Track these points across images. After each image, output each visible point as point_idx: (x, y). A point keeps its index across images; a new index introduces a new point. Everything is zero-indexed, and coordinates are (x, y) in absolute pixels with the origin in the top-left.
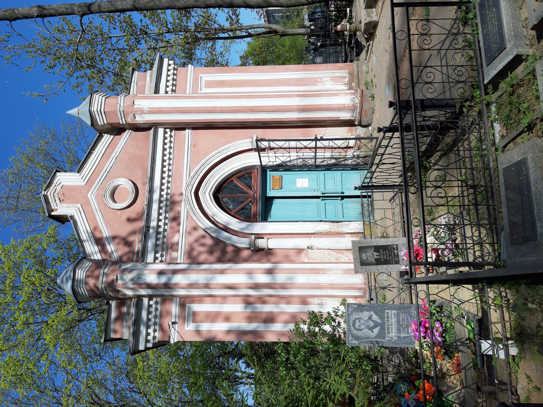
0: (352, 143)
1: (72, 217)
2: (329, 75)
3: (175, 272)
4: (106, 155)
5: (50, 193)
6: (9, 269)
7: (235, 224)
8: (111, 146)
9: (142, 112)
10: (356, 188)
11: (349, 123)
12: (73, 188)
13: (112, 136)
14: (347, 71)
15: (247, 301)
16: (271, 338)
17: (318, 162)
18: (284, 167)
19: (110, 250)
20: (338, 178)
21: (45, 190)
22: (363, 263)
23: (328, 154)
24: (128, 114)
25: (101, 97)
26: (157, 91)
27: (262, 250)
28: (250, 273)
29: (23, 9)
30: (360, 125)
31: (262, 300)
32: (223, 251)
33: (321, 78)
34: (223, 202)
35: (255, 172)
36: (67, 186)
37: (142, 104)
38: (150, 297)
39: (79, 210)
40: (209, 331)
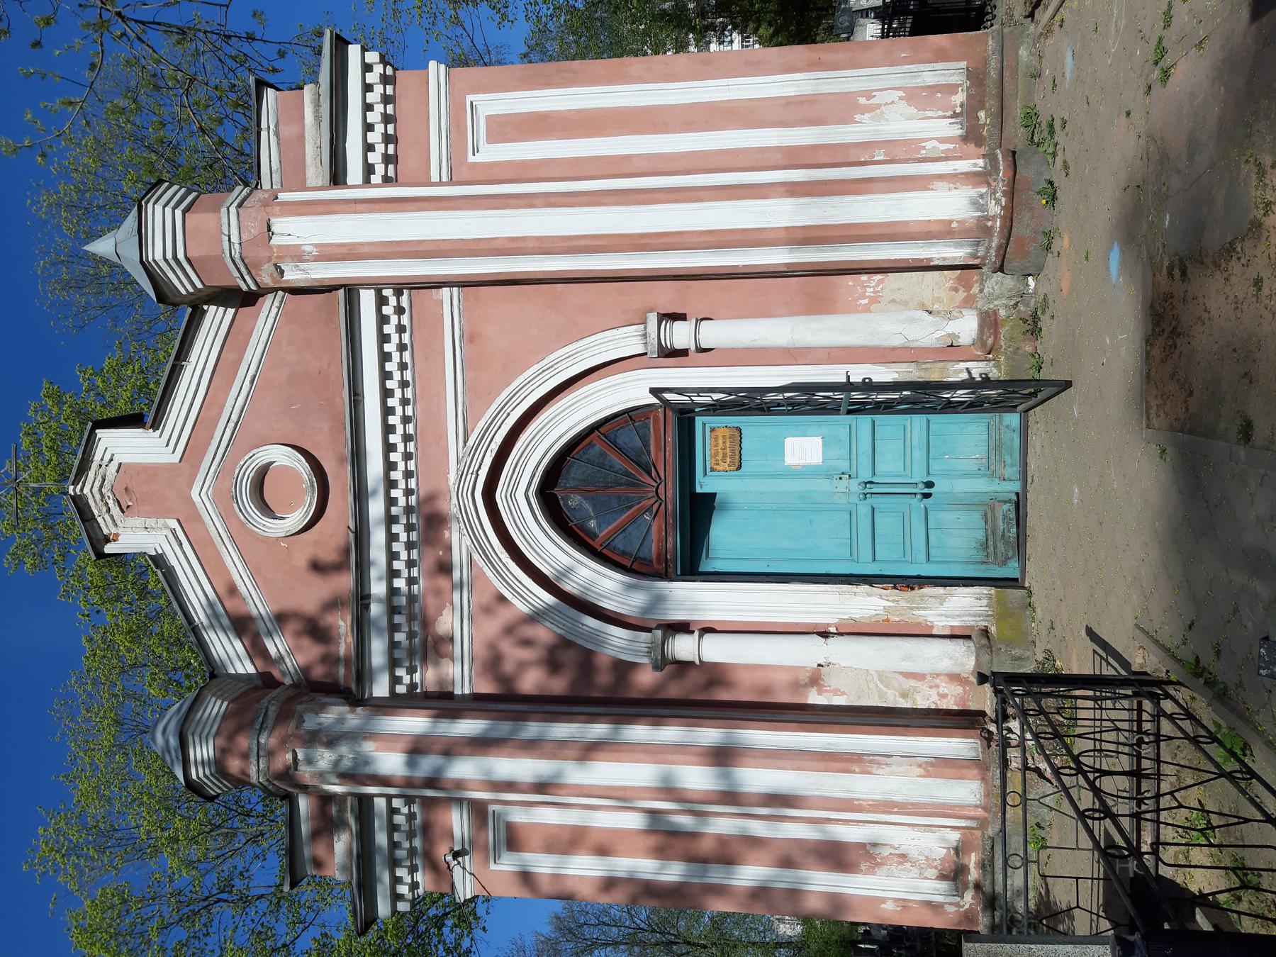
1: (159, 560)
2: (898, 83)
4: (223, 369)
5: (89, 488)
7: (605, 585)
8: (233, 341)
9: (297, 255)
12: (149, 472)
13: (231, 311)
14: (963, 64)
18: (749, 403)
19: (273, 651)
20: (915, 436)
21: (75, 483)
24: (258, 265)
25: (168, 210)
26: (337, 176)
33: (869, 94)
34: (566, 505)
35: (656, 420)
36: (130, 466)
39: (176, 538)
40: (556, 877)
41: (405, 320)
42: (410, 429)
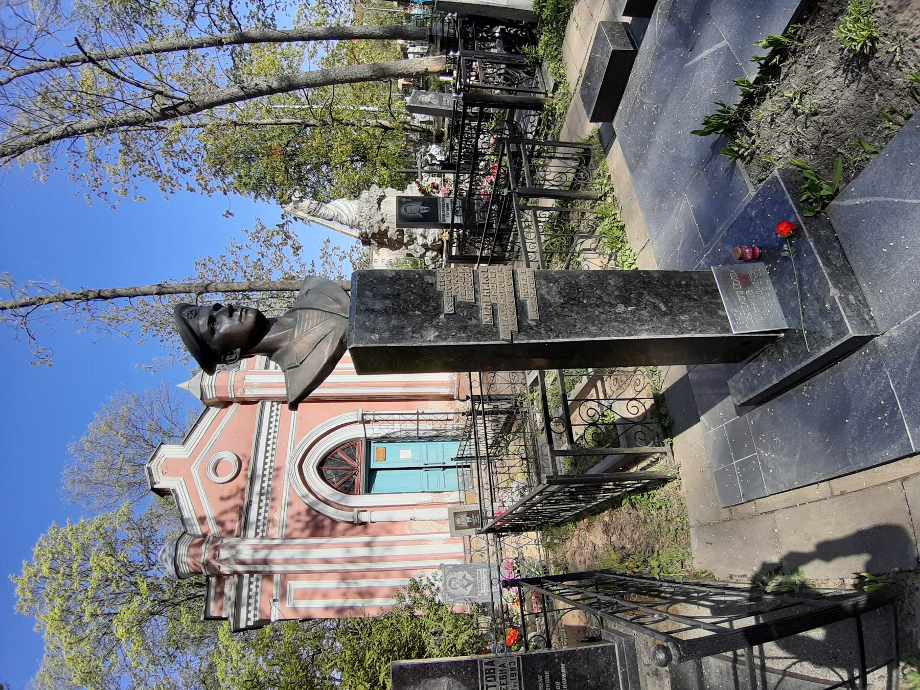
0: (451, 417)
1: (174, 490)
3: (270, 548)
5: (153, 465)
6: (77, 551)
9: (252, 386)
10: (452, 459)
11: (450, 398)
15: (345, 576)
16: (373, 613)
17: (421, 434)
22: (458, 528)
23: (429, 426)
24: (238, 389)
27: (364, 524)
28: (347, 546)
29: (144, 288)
30: (458, 399)
31: (363, 574)
32: (317, 525)
36: (170, 459)
37: (251, 379)
38: (251, 573)
41: (279, 412)
42: (274, 446)
